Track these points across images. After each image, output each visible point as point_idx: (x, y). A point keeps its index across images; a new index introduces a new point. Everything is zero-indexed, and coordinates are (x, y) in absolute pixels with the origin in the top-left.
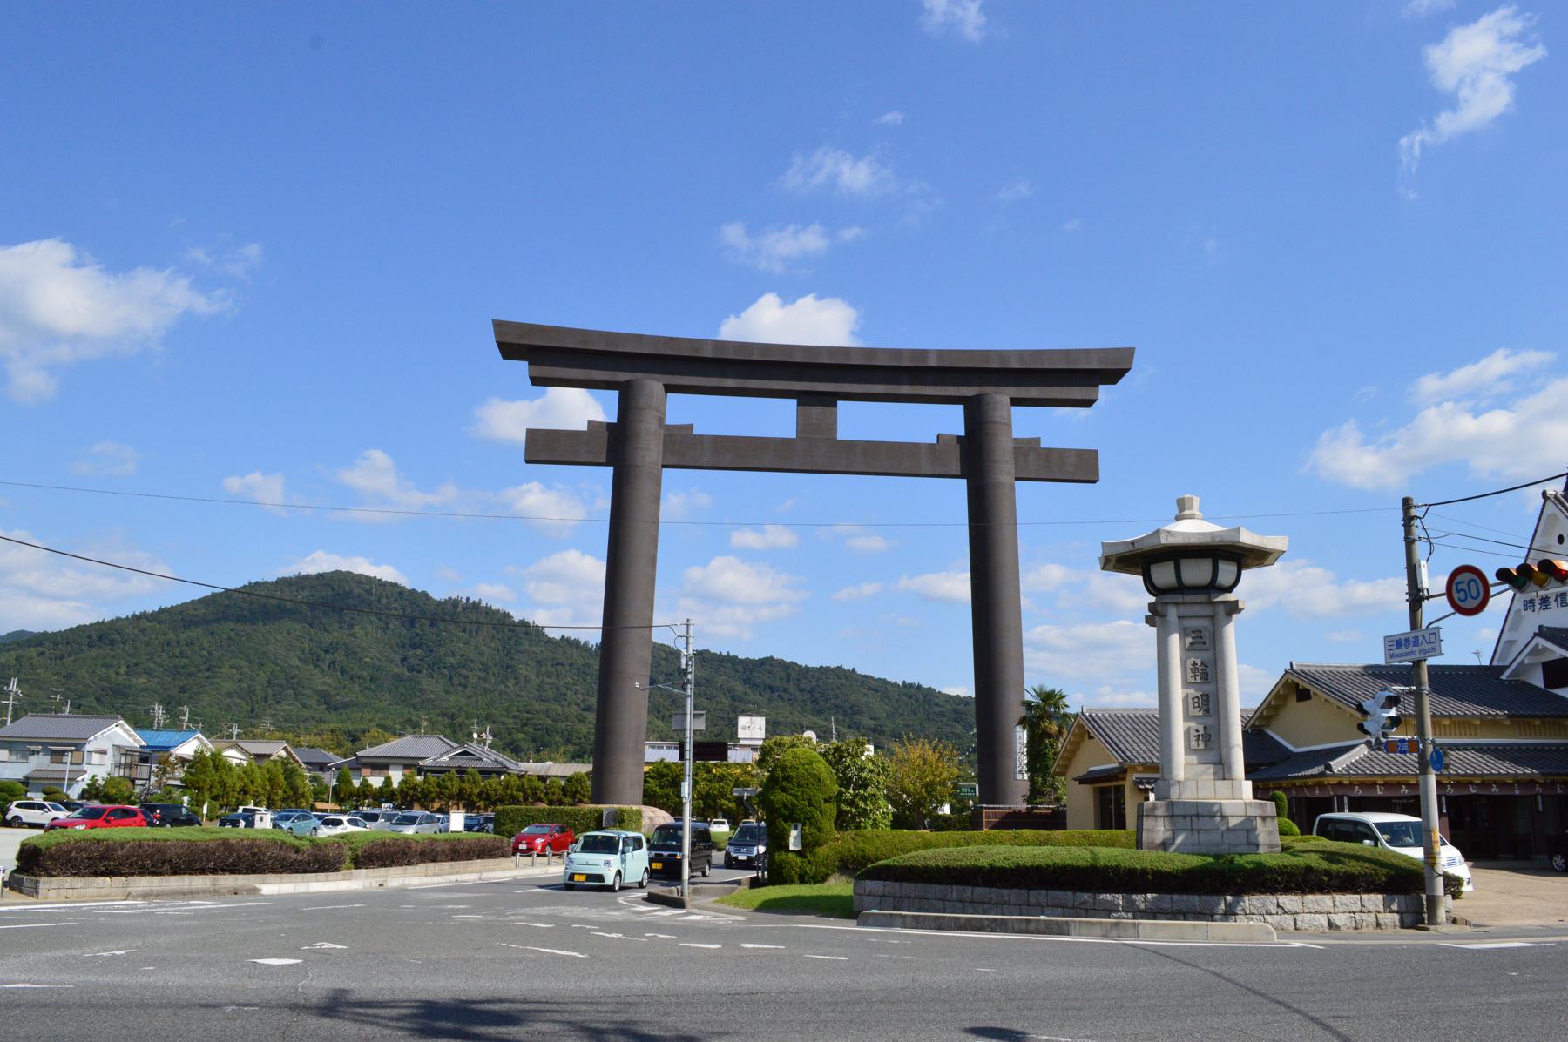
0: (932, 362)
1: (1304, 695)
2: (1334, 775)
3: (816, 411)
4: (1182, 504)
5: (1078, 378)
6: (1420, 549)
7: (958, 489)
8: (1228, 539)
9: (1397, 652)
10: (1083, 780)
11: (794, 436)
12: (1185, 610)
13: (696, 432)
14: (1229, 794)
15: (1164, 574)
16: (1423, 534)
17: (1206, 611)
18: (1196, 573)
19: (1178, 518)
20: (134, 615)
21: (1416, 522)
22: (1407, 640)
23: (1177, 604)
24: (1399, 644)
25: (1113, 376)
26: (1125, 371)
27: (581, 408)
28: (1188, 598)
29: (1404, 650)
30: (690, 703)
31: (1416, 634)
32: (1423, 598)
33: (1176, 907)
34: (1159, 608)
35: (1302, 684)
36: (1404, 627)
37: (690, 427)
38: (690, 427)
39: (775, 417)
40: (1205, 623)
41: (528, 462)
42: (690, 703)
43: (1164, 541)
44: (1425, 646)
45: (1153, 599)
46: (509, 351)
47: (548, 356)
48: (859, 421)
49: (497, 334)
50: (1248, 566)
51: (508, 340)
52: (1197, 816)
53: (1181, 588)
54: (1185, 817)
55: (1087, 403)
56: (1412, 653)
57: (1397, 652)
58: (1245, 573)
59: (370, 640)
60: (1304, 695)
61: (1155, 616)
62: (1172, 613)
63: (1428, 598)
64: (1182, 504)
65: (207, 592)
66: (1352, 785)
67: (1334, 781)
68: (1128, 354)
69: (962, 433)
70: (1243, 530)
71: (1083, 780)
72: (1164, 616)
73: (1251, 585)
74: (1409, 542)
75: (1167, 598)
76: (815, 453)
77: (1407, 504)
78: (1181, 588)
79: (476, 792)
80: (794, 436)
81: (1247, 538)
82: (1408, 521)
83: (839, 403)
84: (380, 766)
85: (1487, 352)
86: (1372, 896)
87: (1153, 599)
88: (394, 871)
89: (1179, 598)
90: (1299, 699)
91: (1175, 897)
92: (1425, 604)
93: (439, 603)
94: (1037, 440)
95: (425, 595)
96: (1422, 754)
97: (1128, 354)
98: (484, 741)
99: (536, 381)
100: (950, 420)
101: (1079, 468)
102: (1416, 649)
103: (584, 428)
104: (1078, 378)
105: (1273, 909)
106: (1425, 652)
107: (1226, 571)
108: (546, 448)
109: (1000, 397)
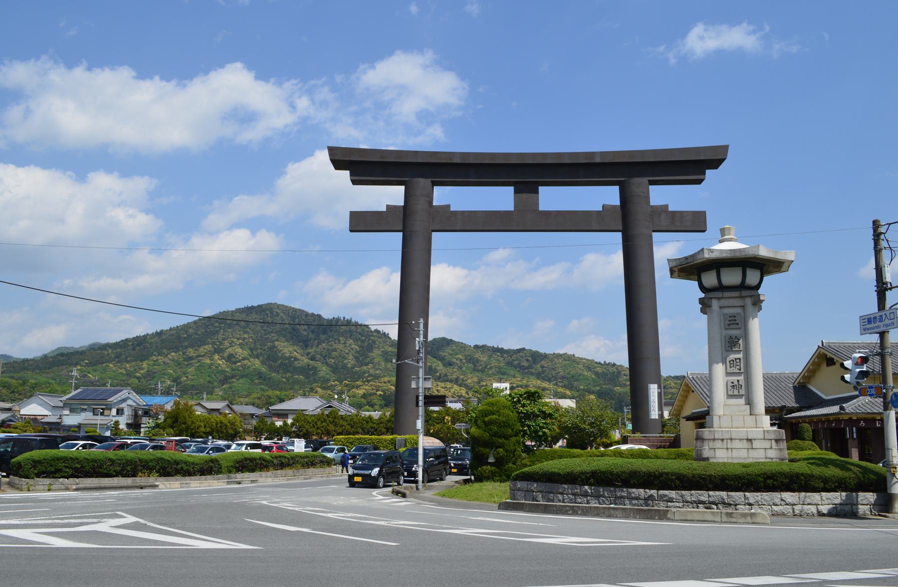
0: (598, 160)
1: (830, 362)
2: (847, 413)
3: (524, 196)
4: (723, 231)
5: (691, 167)
6: (885, 255)
7: (617, 238)
8: (751, 253)
9: (868, 326)
10: (688, 419)
11: (512, 209)
12: (724, 302)
13: (452, 209)
14: (753, 424)
15: (710, 279)
16: (887, 246)
17: (738, 302)
18: (731, 277)
19: (721, 242)
20: (157, 332)
21: (882, 237)
22: (875, 318)
23: (718, 298)
24: (869, 321)
25: (715, 163)
26: (721, 161)
27: (391, 195)
28: (727, 294)
29: (873, 325)
30: (421, 371)
31: (882, 313)
32: (886, 289)
33: (711, 499)
34: (706, 301)
35: (829, 355)
36: (872, 307)
37: (449, 206)
38: (449, 206)
39: (500, 198)
40: (739, 310)
41: (351, 231)
42: (421, 371)
43: (707, 255)
44: (887, 322)
45: (702, 295)
46: (338, 164)
47: (363, 166)
48: (552, 198)
49: (331, 155)
50: (769, 273)
51: (337, 158)
52: (731, 439)
53: (721, 288)
54: (722, 440)
55: (699, 182)
56: (878, 327)
57: (868, 326)
58: (766, 279)
59: (348, 348)
60: (830, 362)
61: (705, 305)
62: (715, 304)
63: (890, 289)
64: (723, 231)
65: (191, 319)
66: (859, 420)
67: (846, 417)
68: (725, 148)
69: (511, 189)
70: (761, 247)
71: (688, 419)
72: (710, 306)
73: (770, 285)
74: (877, 252)
75: (711, 295)
76: (526, 220)
77: (876, 224)
78: (721, 288)
79: (123, 422)
80: (512, 209)
81: (764, 252)
82: (877, 236)
83: (541, 188)
84: (283, 415)
85: (732, 20)
86: (738, 493)
87: (702, 295)
88: (107, 479)
89: (719, 294)
90: (828, 365)
91: (711, 493)
92: (888, 293)
93: (328, 320)
94: (667, 206)
95: (319, 316)
96: (885, 396)
97: (725, 148)
98: (343, 400)
99: (354, 182)
100: (610, 195)
101: (694, 222)
102: (881, 324)
103: (385, 210)
104: (691, 167)
105: (778, 501)
106: (887, 325)
107: (752, 277)
108: (362, 222)
109: (639, 182)
